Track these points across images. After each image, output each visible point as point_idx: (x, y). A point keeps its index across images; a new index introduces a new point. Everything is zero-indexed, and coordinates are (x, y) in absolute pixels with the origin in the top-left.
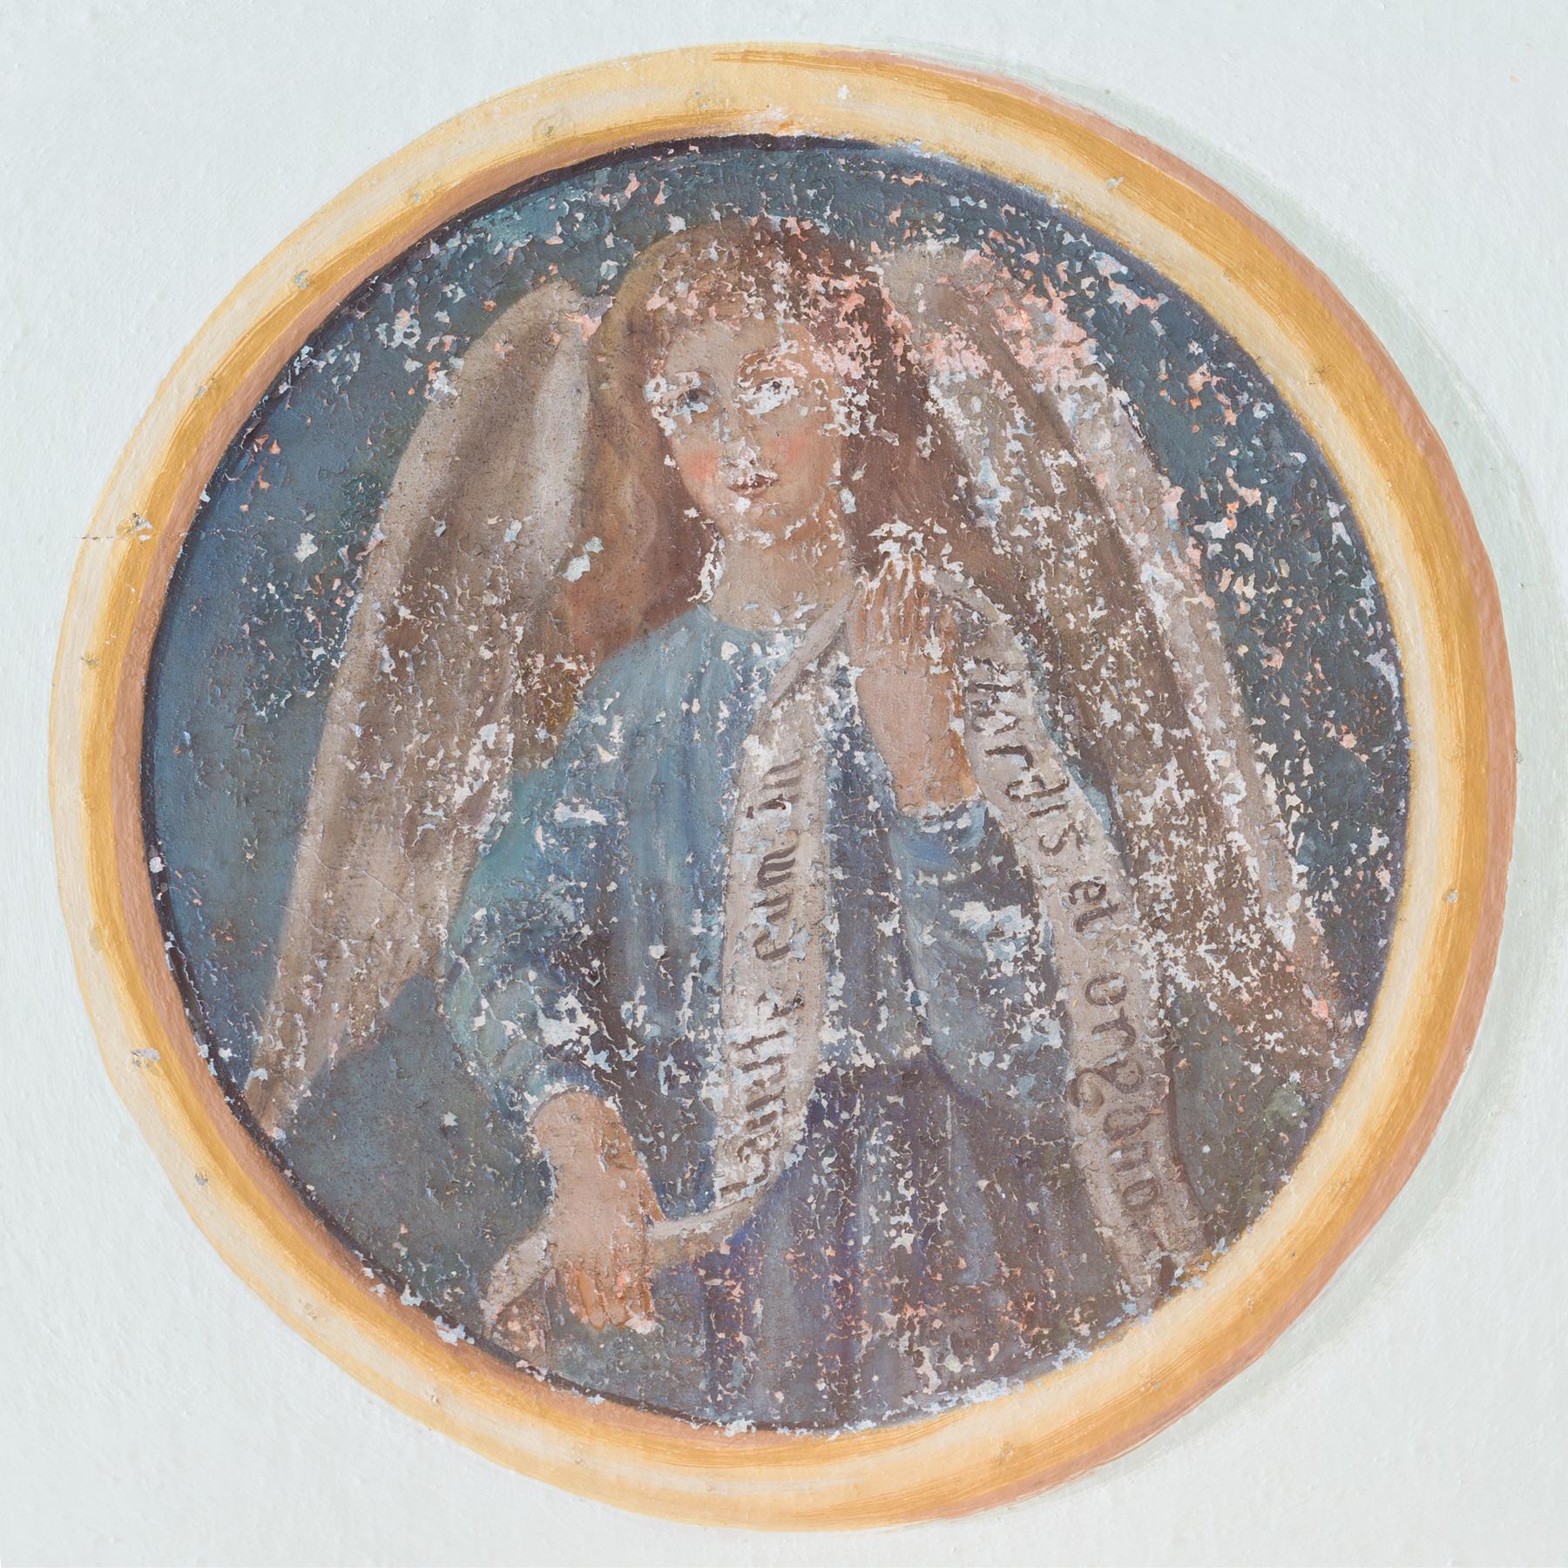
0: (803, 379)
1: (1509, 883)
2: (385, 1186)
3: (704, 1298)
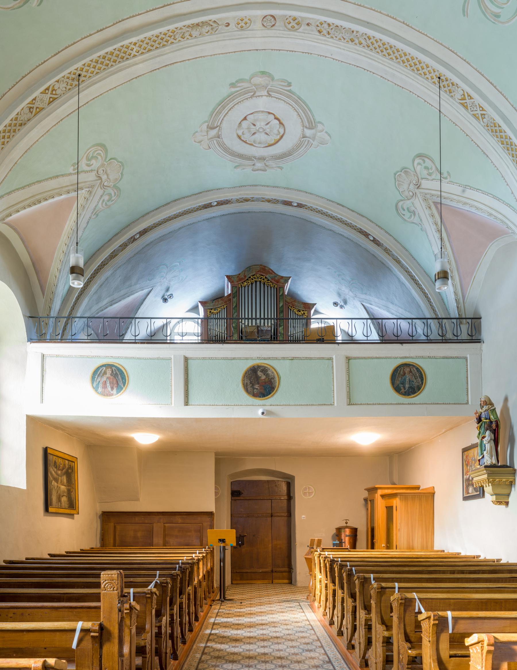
0: (408, 369)
1: (117, 625)
2: (397, 389)
3: (405, 392)
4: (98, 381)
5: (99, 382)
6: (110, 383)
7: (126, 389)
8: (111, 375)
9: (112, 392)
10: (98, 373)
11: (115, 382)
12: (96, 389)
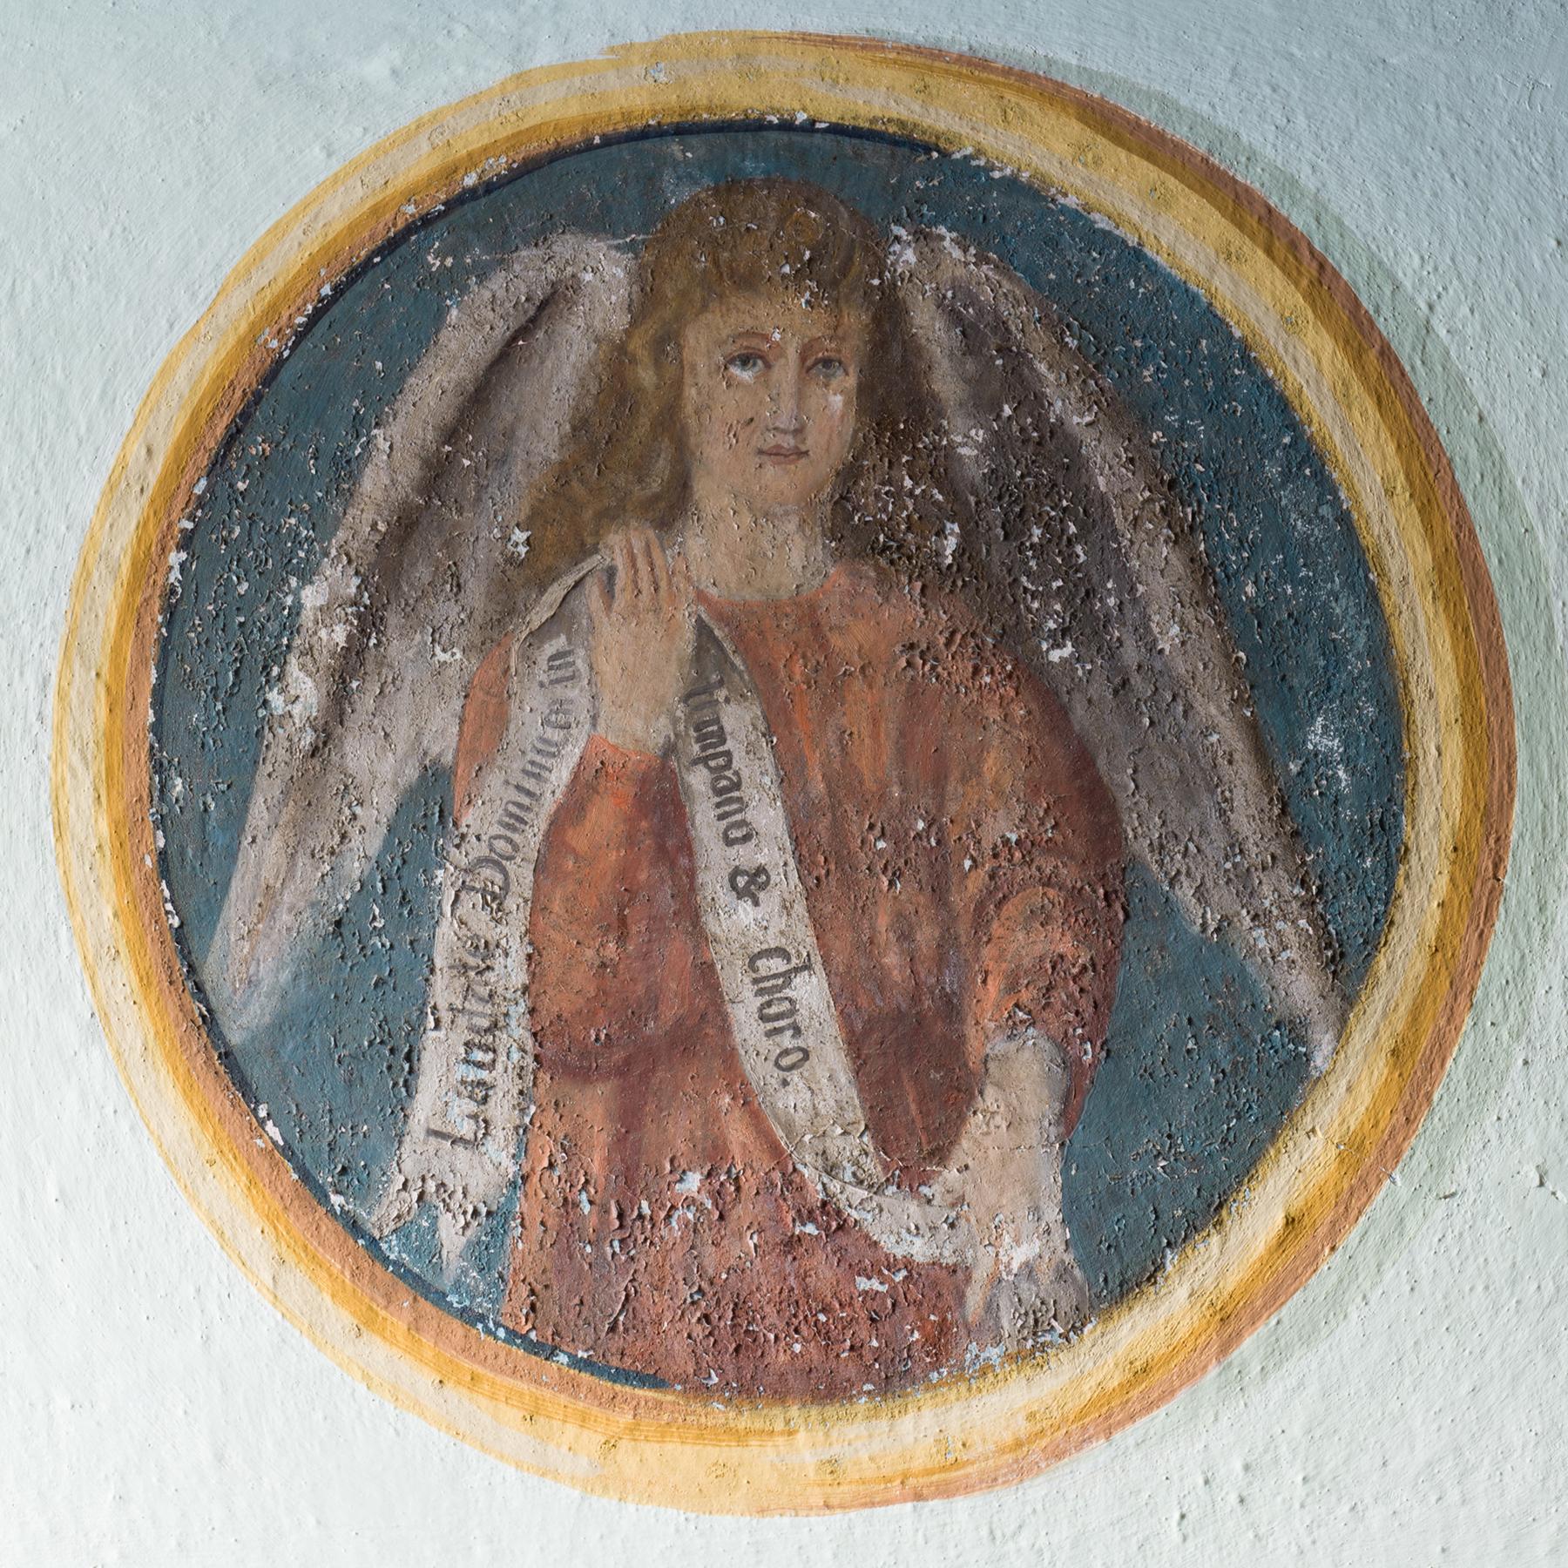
4: (377, 767)
5: (430, 803)
6: (824, 859)
7: (1417, 1067)
8: (849, 526)
9: (901, 1228)
10: (386, 472)
11: (998, 808)
12: (302, 1087)
